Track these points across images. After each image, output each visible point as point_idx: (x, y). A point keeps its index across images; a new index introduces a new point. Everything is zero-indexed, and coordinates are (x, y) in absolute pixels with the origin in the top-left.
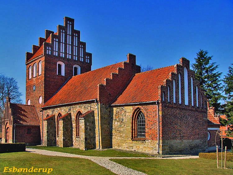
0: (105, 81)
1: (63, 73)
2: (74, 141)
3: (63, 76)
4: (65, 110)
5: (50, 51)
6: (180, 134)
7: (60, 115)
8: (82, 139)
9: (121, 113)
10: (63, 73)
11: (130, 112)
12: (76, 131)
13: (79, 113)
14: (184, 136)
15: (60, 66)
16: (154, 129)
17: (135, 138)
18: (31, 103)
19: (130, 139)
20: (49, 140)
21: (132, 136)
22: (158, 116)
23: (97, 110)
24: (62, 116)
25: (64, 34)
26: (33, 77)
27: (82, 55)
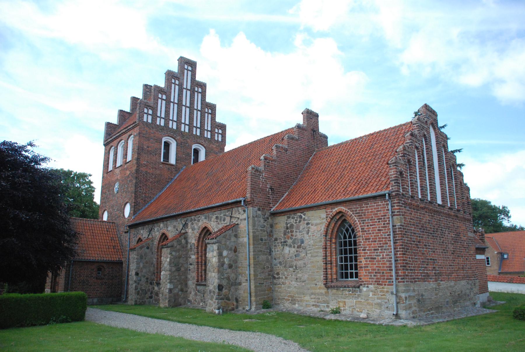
0: (263, 161)
1: (172, 160)
2: (193, 293)
3: (172, 165)
4: (174, 227)
5: (150, 118)
6: (434, 268)
7: (164, 237)
8: (211, 287)
9: (298, 228)
10: (172, 160)
11: (321, 223)
12: (198, 270)
13: (206, 232)
14: (440, 274)
15: (167, 145)
16: (383, 258)
17: (202, 280)
18: (108, 217)
19: (321, 284)
20: (139, 291)
21: (326, 279)
22: (391, 227)
23: (246, 221)
24: (168, 239)
25: (177, 87)
26: (115, 166)
27: (208, 126)
